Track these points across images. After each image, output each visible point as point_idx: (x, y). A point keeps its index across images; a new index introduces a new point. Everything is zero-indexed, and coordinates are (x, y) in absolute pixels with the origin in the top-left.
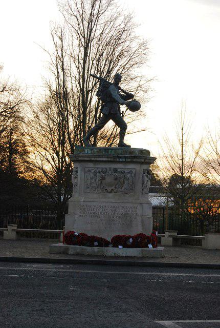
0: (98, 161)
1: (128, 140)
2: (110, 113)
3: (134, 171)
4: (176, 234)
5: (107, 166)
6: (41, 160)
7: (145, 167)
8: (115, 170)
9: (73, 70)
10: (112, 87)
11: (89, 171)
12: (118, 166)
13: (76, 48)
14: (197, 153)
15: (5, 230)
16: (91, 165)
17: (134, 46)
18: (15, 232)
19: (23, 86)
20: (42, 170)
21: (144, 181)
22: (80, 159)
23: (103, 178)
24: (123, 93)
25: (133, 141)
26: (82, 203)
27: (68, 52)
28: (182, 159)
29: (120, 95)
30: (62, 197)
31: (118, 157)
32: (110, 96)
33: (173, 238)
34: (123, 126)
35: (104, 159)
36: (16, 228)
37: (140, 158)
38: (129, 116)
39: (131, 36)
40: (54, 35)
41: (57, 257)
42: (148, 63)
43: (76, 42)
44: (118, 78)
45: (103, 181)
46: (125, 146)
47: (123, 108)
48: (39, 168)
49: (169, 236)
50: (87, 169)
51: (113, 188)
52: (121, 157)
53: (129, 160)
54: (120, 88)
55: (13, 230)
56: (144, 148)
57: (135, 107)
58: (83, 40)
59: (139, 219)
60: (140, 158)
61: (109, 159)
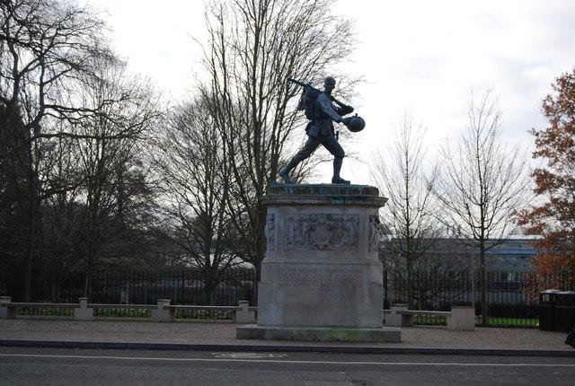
0: (307, 204)
1: (344, 175)
2: (320, 134)
3: (356, 218)
4: (405, 309)
5: (318, 211)
6: (176, 200)
7: (371, 211)
8: (329, 217)
9: (239, 69)
10: (321, 97)
11: (291, 219)
12: (335, 211)
13: (243, 35)
14: (430, 188)
15: (76, 307)
16: (293, 210)
17: (330, 30)
18: (400, 316)
19: (156, 91)
20: (181, 216)
21: (371, 232)
22: (278, 201)
23: (312, 229)
24: (337, 106)
25: (354, 174)
26: (282, 266)
27: (231, 42)
28: (407, 199)
29: (333, 107)
30: (212, 257)
31: (335, 198)
32: (320, 110)
33: (403, 315)
34: (339, 155)
35: (313, 202)
36: (168, 305)
37: (364, 199)
38: (346, 140)
39: (325, 16)
40: (209, 13)
41: (246, 343)
42: (350, 56)
43: (242, 26)
44: (330, 83)
45: (312, 234)
46: (343, 181)
47: (339, 127)
48: (176, 214)
49: (398, 313)
50: (288, 216)
51: (326, 243)
52: (338, 198)
53: (350, 202)
54: (333, 99)
55: (165, 308)
56: (370, 185)
57: (357, 125)
58: (252, 22)
59: (366, 288)
60: (364, 199)
61: (321, 202)
